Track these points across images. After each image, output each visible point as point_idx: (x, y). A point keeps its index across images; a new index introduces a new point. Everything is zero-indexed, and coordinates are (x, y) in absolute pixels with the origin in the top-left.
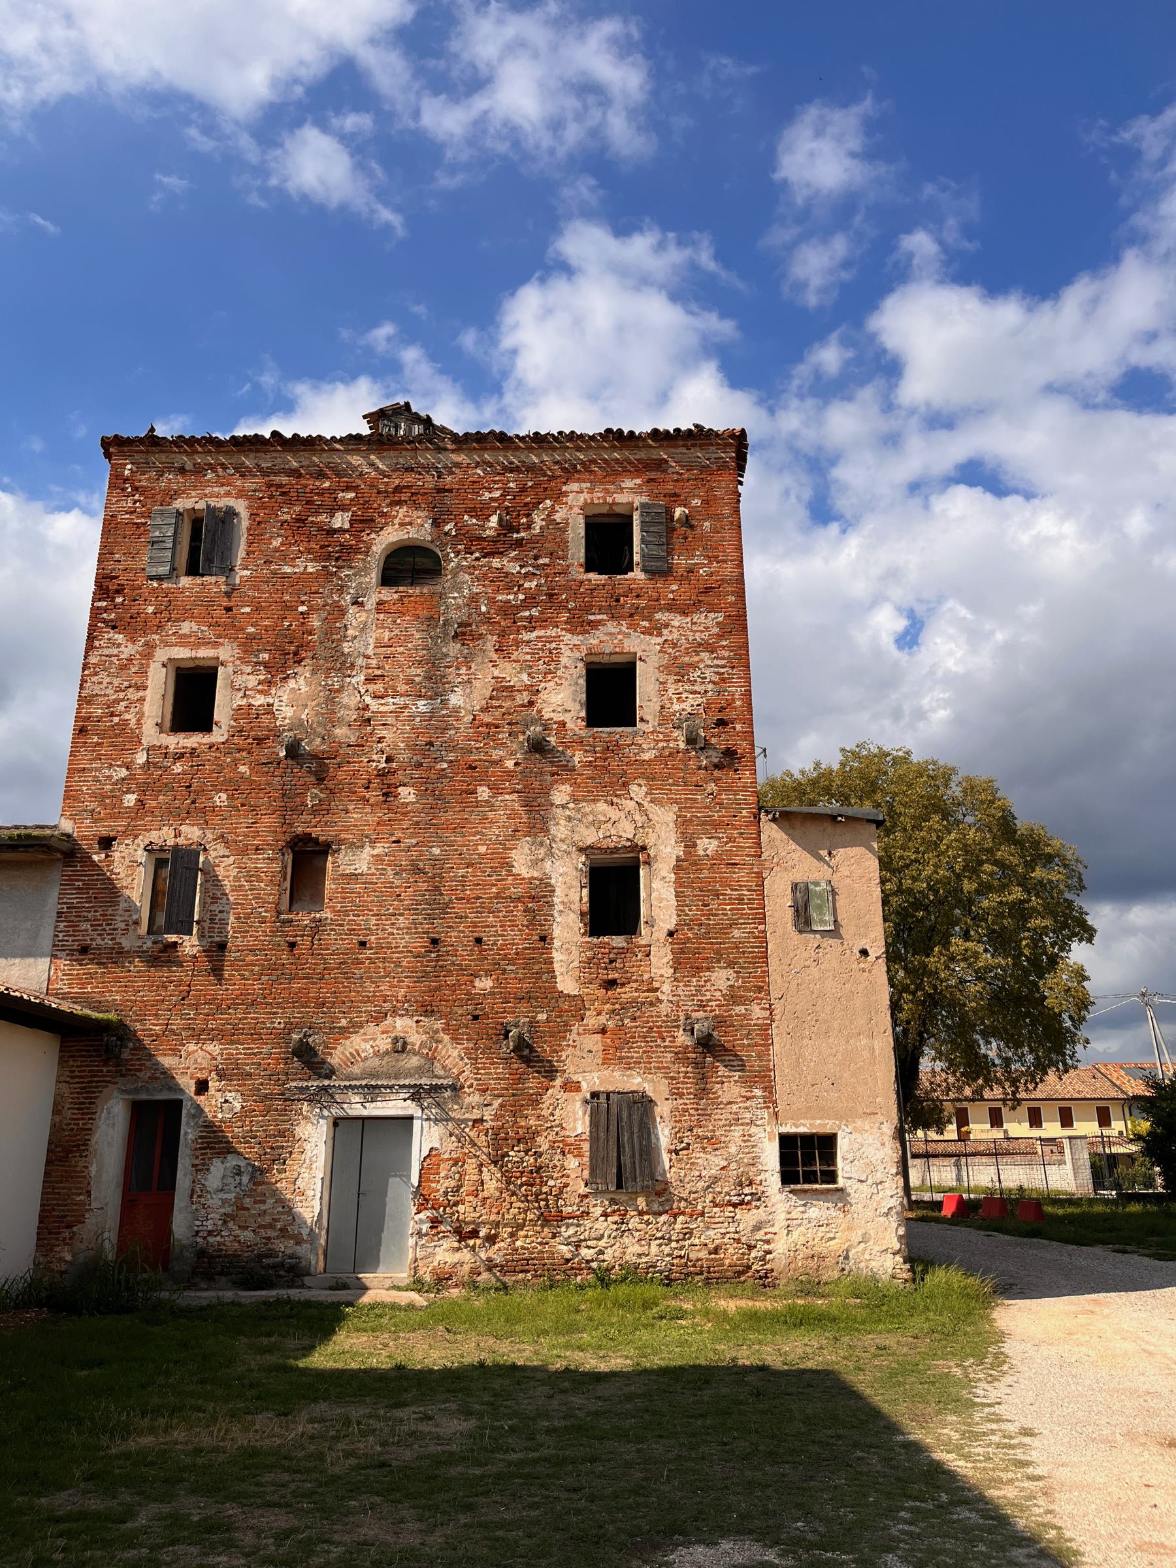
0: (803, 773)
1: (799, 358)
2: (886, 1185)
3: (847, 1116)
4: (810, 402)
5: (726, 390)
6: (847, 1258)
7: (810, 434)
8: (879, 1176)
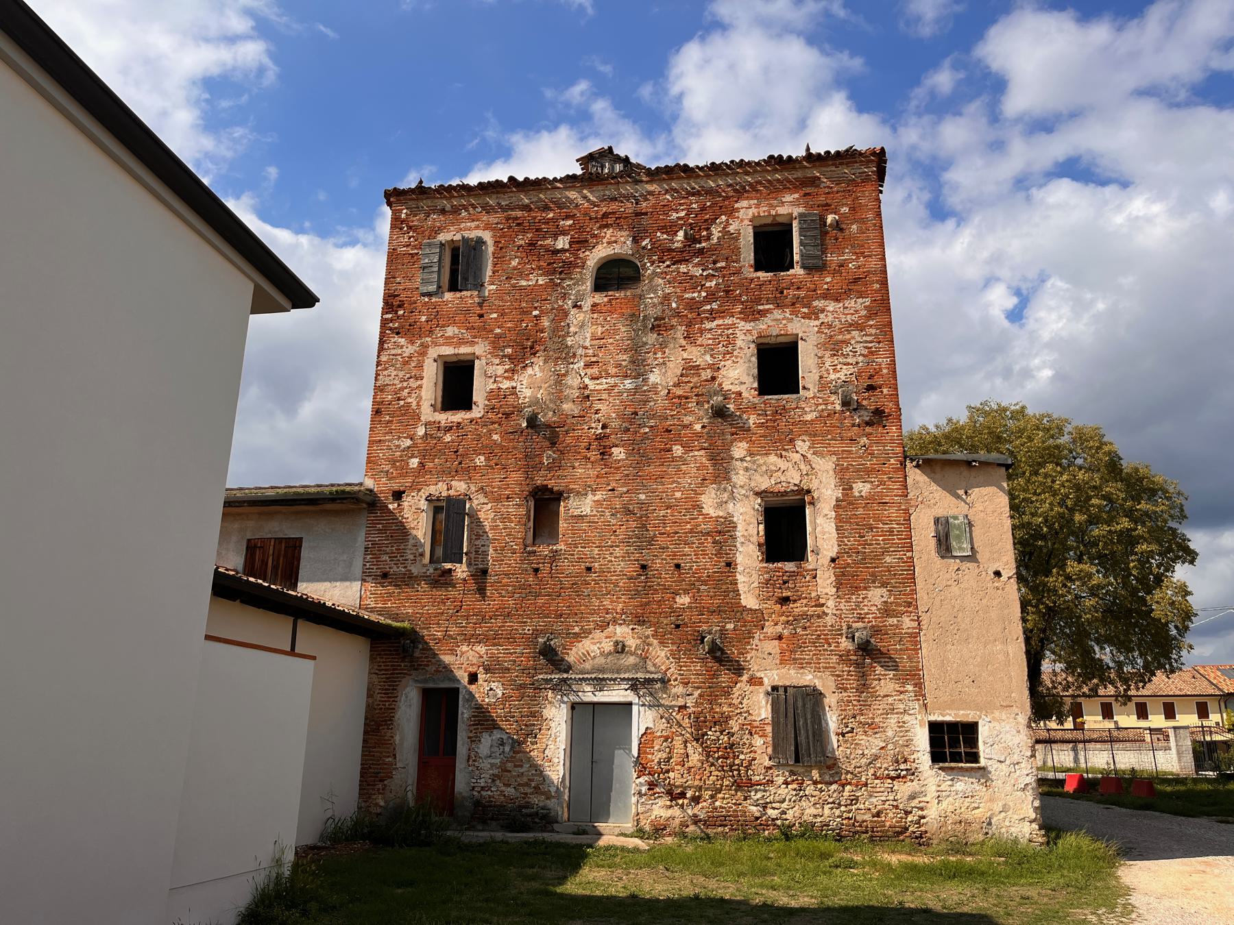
0: (937, 427)
1: (916, 82)
2: (1023, 765)
3: (987, 708)
4: (927, 119)
5: (854, 114)
6: (990, 824)
7: (926, 147)
8: (1016, 758)
